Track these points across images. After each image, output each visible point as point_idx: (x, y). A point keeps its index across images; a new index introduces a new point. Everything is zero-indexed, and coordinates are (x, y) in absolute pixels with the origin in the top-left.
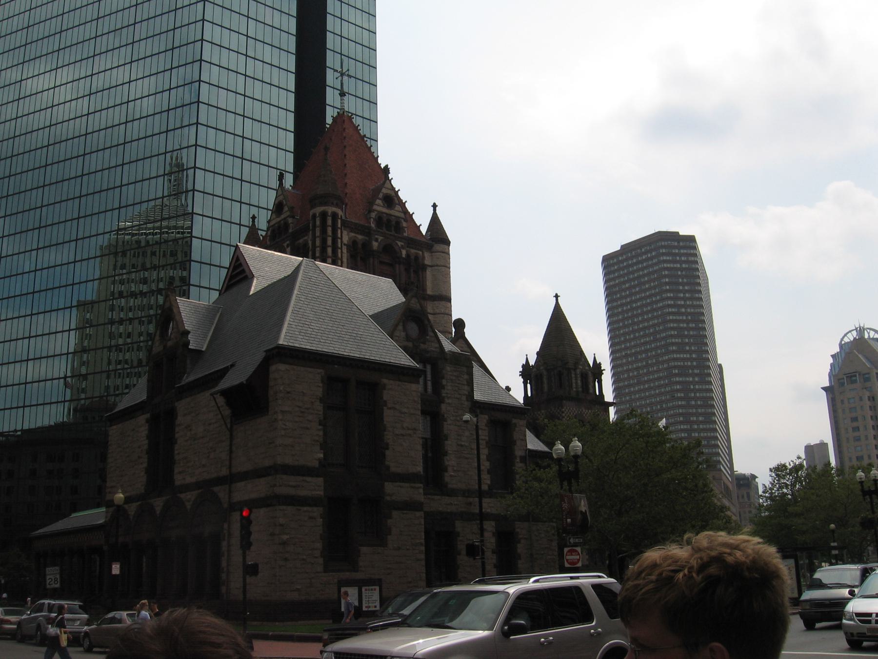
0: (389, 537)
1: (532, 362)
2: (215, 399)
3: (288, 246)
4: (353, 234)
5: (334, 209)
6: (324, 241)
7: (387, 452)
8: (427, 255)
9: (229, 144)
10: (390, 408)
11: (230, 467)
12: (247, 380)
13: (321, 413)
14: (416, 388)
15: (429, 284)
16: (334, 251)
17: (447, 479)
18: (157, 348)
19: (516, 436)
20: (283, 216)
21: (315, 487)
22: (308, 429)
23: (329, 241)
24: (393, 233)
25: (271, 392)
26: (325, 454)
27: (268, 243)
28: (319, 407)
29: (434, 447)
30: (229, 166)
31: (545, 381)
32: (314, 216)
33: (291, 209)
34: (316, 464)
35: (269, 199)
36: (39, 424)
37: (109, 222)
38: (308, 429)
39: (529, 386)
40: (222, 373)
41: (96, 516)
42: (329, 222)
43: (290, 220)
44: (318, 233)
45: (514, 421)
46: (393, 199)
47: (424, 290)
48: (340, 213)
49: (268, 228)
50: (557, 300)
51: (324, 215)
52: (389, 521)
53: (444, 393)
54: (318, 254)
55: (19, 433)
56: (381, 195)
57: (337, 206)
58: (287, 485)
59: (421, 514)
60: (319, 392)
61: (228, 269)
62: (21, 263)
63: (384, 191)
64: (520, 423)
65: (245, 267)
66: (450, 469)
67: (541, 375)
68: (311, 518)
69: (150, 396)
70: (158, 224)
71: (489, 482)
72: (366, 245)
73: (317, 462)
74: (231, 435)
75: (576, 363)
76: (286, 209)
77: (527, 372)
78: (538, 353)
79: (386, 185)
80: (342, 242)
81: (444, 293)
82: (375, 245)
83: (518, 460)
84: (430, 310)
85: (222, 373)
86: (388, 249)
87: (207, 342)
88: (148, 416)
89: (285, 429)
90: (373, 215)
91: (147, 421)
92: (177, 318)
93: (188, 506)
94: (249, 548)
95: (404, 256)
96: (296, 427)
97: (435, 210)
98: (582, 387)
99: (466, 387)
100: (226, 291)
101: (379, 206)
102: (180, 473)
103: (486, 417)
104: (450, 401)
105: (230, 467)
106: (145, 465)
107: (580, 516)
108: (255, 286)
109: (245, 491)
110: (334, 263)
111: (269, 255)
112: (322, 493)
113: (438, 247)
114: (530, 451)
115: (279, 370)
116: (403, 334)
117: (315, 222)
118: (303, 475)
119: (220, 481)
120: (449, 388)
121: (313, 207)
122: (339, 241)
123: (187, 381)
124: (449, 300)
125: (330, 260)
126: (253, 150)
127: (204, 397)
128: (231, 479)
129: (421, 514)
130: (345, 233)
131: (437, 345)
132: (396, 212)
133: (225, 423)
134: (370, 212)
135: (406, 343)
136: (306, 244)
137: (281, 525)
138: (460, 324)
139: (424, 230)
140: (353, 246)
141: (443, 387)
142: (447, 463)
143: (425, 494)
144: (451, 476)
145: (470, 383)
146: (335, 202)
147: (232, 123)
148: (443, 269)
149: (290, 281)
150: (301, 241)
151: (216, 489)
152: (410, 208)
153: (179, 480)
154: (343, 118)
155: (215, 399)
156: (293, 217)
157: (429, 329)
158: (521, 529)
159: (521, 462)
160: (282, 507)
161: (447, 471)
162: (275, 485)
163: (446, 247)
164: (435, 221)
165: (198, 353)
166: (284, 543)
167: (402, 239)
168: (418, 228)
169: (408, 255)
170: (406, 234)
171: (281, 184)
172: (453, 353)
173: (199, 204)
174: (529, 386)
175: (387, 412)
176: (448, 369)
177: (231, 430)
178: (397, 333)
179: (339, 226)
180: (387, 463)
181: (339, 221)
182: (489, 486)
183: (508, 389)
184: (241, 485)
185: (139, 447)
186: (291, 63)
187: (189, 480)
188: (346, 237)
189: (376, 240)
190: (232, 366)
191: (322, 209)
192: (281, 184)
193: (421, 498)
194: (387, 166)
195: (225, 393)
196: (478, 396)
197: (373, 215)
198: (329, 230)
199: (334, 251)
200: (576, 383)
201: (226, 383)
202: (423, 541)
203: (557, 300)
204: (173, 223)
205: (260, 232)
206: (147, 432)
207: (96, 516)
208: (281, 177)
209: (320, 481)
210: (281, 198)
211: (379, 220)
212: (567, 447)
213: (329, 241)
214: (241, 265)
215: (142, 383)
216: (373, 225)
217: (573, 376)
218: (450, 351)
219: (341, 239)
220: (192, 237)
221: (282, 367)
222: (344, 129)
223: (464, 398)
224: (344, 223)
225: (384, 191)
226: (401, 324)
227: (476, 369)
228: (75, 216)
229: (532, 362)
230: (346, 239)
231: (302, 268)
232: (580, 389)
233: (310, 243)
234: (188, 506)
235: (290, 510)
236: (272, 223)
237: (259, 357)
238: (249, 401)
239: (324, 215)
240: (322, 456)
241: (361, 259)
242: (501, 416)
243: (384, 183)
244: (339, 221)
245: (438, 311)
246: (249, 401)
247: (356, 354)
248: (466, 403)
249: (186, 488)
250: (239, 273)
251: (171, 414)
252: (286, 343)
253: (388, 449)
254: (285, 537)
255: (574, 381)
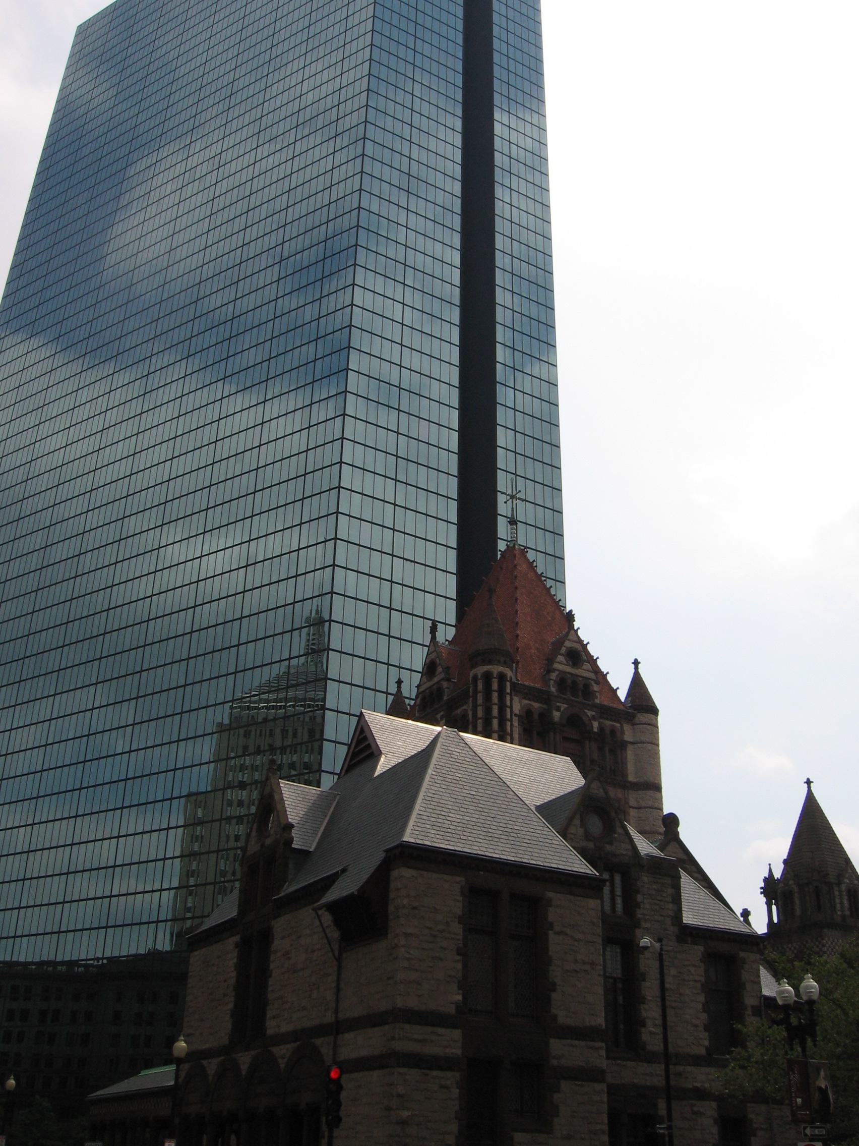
0: (556, 1120)
1: (777, 874)
2: (319, 917)
3: (441, 719)
4: (527, 702)
5: (501, 669)
6: (488, 711)
7: (554, 995)
8: (627, 728)
9: (373, 590)
10: (558, 933)
11: (337, 1011)
12: (358, 890)
13: (460, 937)
14: (592, 908)
15: (631, 768)
16: (502, 724)
17: (645, 1037)
18: (254, 847)
19: (745, 976)
20: (436, 680)
21: (449, 1042)
22: (441, 959)
23: (495, 711)
24: (580, 699)
25: (391, 908)
26: (464, 998)
27: (417, 714)
28: (457, 929)
29: (624, 993)
30: (374, 618)
31: (797, 901)
32: (475, 678)
33: (447, 669)
34: (452, 1010)
35: (417, 658)
36: (133, 951)
37: (223, 690)
38: (441, 959)
39: (774, 908)
40: (330, 881)
41: (161, 1076)
42: (495, 686)
43: (445, 684)
44: (480, 700)
45: (742, 954)
46: (579, 654)
47: (625, 775)
48: (509, 673)
49: (417, 697)
50: (809, 787)
51: (488, 677)
52: (556, 1096)
53: (639, 914)
54: (480, 728)
55: (105, 961)
56: (563, 650)
57: (505, 664)
58: (410, 1039)
59: (604, 1086)
60: (458, 908)
61: (349, 746)
62: (113, 741)
63: (568, 644)
64: (750, 957)
65: (371, 741)
66: (649, 1023)
67: (791, 893)
68: (442, 1087)
69: (242, 912)
70: (282, 695)
71: (706, 1043)
72: (544, 717)
73: (453, 1006)
74: (340, 968)
75: (840, 876)
76: (440, 669)
77: (771, 889)
78: (785, 862)
79: (570, 637)
80: (512, 712)
81: (651, 780)
82: (556, 715)
83: (749, 1012)
84: (632, 802)
85: (330, 881)
86: (574, 721)
87: (317, 840)
88: (237, 938)
89: (408, 959)
90: (553, 676)
91: (237, 945)
92: (279, 807)
93: (282, 1063)
94: (337, 1126)
95: (595, 730)
96: (424, 958)
97: (636, 668)
98: (850, 909)
99: (671, 906)
100: (348, 771)
101: (561, 665)
102: (274, 1017)
103: (701, 948)
104: (648, 925)
105: (337, 1011)
106: (231, 1006)
107: (817, 1095)
108: (383, 765)
109: (360, 1044)
110: (501, 739)
111: (427, 729)
112: (458, 1052)
113: (642, 717)
114: (767, 998)
115: (402, 875)
116: (581, 831)
117: (476, 686)
118: (433, 1025)
119: (322, 1030)
120: (648, 906)
121: (473, 666)
122: (508, 710)
123: (287, 892)
124: (658, 788)
125: (495, 735)
126: (405, 599)
127: (306, 915)
128: (338, 1028)
129: (604, 1086)
130: (516, 699)
131: (629, 847)
132: (584, 672)
133: (332, 951)
134: (549, 671)
135: (584, 844)
136: (464, 717)
137: (399, 1096)
138: (672, 821)
139: (622, 695)
140: (527, 717)
141: (638, 905)
142: (644, 1014)
143: (608, 1058)
144: (651, 1033)
145: (677, 900)
146: (502, 659)
147: (379, 564)
148: (650, 747)
149: (423, 758)
150: (459, 711)
151: (318, 1042)
152: (603, 665)
153: (272, 1027)
154: (516, 552)
155: (319, 917)
156: (448, 680)
157: (618, 824)
158: (756, 1114)
159: (754, 1015)
160: (402, 1070)
161: (644, 1026)
162: (393, 1038)
163: (653, 716)
164: (637, 683)
165: (304, 854)
166: (404, 1123)
167: (594, 707)
168: (614, 692)
169: (601, 729)
170: (597, 701)
171: (434, 638)
172: (652, 858)
173: (335, 666)
174: (774, 908)
175: (553, 938)
176: (645, 879)
177: (339, 960)
178: (572, 830)
179: (508, 690)
180: (553, 1011)
181: (508, 684)
182: (707, 1048)
183: (746, 913)
184: (349, 1036)
185: (225, 981)
186: (452, 487)
187: (285, 1028)
188: (517, 705)
189: (558, 709)
190: (344, 871)
191: (486, 668)
192: (434, 638)
193: (604, 1063)
194: (571, 611)
195: (332, 907)
196: (688, 918)
197: (553, 676)
198: (495, 696)
199: (502, 724)
200: (841, 903)
201: (333, 894)
202: (606, 1128)
203: (809, 787)
204: (300, 693)
205: (407, 701)
206: (235, 960)
207: (161, 1076)
208: (434, 630)
209: (457, 1034)
210: (433, 656)
211: (563, 683)
212: (796, 988)
213: (495, 711)
214: (365, 738)
215: (234, 897)
216: (553, 689)
217: (837, 893)
218: (647, 855)
219: (511, 707)
220: (323, 708)
221: (407, 873)
222: (515, 566)
223: (668, 921)
224: (514, 686)
225: (568, 644)
226: (578, 816)
227: (686, 881)
228: (189, 688)
229: (777, 874)
230: (517, 708)
231: (439, 745)
232: (848, 913)
233: (470, 713)
234: (282, 1063)
235: (413, 1074)
236: (421, 689)
237: (377, 858)
238: (362, 918)
239: (488, 677)
240: (460, 997)
241: (537, 734)
242: (728, 948)
243: (568, 633)
244: (508, 684)
245: (643, 804)
246: (362, 918)
247: (509, 856)
248: (672, 928)
249: (280, 1039)
250: (363, 748)
251: (266, 936)
252: (412, 840)
253: (554, 990)
254: (405, 1114)
255: (838, 901)
